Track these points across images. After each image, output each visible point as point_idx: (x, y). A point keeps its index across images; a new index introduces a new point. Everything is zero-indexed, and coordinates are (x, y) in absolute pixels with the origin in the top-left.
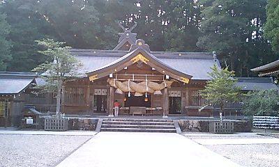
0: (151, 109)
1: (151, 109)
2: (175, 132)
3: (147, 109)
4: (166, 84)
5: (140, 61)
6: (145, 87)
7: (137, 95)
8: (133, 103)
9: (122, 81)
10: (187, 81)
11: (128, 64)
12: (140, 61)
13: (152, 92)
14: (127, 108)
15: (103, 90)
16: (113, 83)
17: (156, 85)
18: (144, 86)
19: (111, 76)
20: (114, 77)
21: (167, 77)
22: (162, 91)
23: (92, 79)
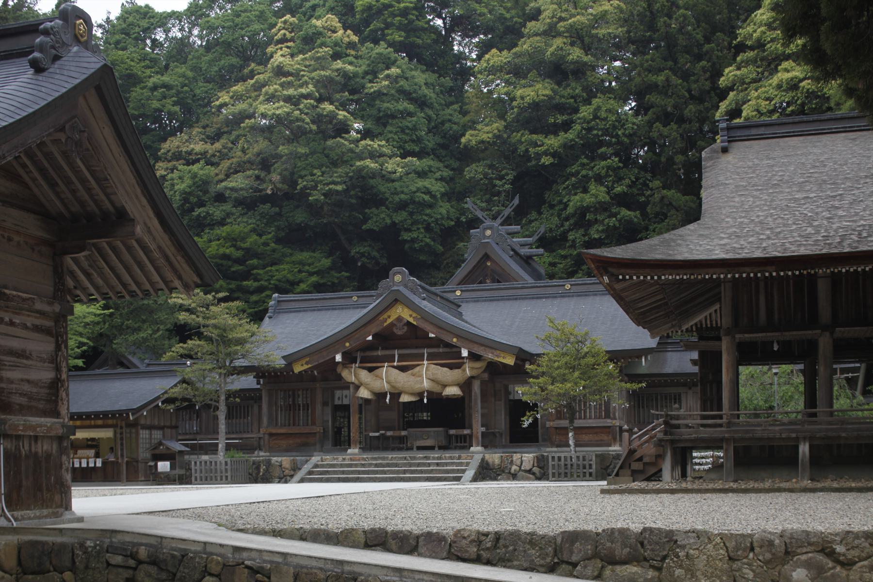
3: (452, 432)
5: (399, 319)
6: (425, 377)
7: (405, 398)
11: (375, 328)
12: (399, 319)
13: (437, 389)
14: (403, 433)
16: (349, 375)
19: (338, 358)
21: (465, 353)
23: (298, 368)
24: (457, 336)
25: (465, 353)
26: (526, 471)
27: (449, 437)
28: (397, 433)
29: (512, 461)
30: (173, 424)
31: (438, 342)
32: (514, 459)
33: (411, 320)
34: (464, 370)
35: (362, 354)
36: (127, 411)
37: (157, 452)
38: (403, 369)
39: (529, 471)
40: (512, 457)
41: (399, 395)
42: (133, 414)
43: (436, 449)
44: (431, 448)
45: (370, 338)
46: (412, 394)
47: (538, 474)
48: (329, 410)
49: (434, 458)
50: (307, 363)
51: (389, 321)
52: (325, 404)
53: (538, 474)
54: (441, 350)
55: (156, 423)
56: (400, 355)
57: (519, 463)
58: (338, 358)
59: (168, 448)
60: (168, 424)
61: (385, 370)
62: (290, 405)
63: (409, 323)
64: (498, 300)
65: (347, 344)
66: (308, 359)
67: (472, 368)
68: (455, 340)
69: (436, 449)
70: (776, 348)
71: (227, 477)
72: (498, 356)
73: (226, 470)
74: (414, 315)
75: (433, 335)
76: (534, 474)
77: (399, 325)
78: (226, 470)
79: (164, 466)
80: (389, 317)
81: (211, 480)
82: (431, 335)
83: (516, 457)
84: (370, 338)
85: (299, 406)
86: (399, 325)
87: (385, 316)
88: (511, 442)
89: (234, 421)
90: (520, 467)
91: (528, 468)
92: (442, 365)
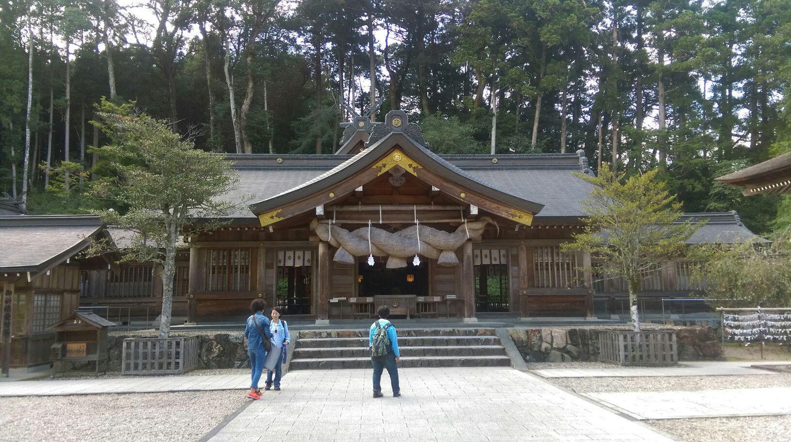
0: (429, 299)
1: (429, 299)
2: (506, 363)
3: (421, 299)
4: (469, 230)
5: (397, 168)
8: (379, 283)
9: (351, 228)
10: (526, 220)
11: (367, 177)
13: (433, 254)
14: (369, 300)
15: (299, 253)
17: (441, 238)
18: (363, 238)
19: (320, 210)
20: (328, 215)
21: (474, 210)
22: (459, 251)
24: (467, 190)
25: (474, 210)
26: (559, 349)
27: (418, 304)
28: (362, 300)
29: (541, 337)
30: (75, 288)
31: (442, 199)
32: (544, 334)
33: (411, 170)
34: (464, 231)
35: (339, 209)
36: (23, 270)
37: (67, 328)
38: (390, 229)
39: (563, 350)
40: (539, 331)
41: (386, 258)
42: (32, 274)
43: (408, 318)
44: (403, 317)
45: (360, 189)
46: (401, 258)
47: (575, 353)
48: (273, 273)
49: (445, 334)
50: (278, 216)
51: (384, 170)
52: (268, 266)
53: (575, 353)
54: (433, 208)
55: (55, 286)
56: (337, 212)
57: (549, 340)
58: (320, 210)
59: (87, 325)
60: (68, 287)
61: (368, 232)
62: (225, 267)
63: (407, 174)
64: (299, 169)
65: (332, 195)
66: (279, 211)
67: (471, 230)
68: (463, 195)
69: (408, 318)
70: (271, 230)
71: (177, 363)
72: (513, 215)
73: (178, 353)
74: (415, 165)
75: (437, 189)
76: (568, 352)
77: (397, 175)
78: (178, 353)
79: (76, 347)
80: (384, 166)
81: (161, 366)
82: (435, 189)
83: (545, 331)
84: (360, 189)
85: (236, 268)
86: (397, 175)
87: (379, 164)
88: (478, 309)
89: (132, 284)
90: (551, 344)
91: (562, 347)
92: (439, 227)
